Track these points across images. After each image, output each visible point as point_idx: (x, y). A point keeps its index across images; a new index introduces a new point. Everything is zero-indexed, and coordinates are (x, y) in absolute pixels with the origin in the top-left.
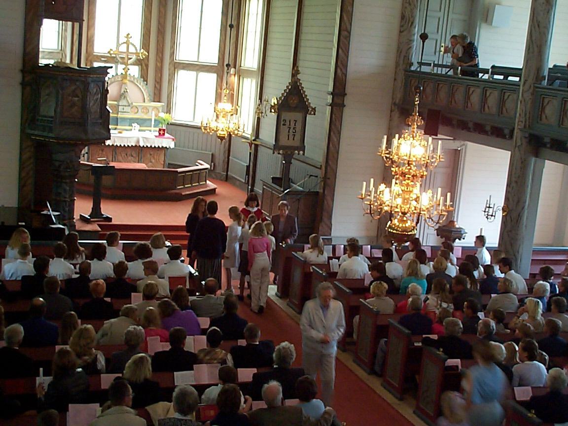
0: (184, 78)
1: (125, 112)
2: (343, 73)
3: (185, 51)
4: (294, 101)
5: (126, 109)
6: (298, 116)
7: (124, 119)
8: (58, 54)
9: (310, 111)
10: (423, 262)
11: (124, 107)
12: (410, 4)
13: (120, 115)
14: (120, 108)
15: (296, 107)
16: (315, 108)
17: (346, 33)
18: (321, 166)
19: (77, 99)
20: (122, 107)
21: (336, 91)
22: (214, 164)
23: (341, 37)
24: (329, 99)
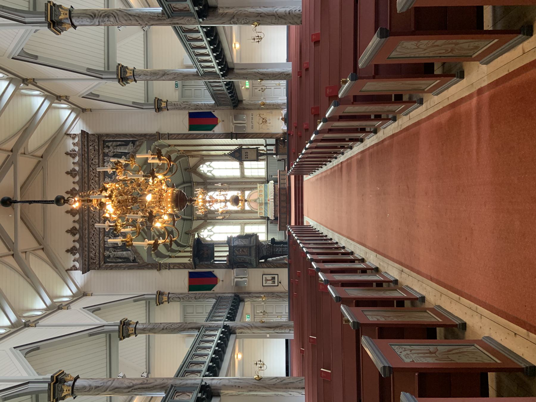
2: (222, 135)
3: (237, 173)
4: (237, 154)
5: (261, 199)
7: (265, 200)
12: (189, 107)
13: (263, 202)
14: (260, 202)
17: (205, 136)
21: (230, 137)
23: (207, 138)
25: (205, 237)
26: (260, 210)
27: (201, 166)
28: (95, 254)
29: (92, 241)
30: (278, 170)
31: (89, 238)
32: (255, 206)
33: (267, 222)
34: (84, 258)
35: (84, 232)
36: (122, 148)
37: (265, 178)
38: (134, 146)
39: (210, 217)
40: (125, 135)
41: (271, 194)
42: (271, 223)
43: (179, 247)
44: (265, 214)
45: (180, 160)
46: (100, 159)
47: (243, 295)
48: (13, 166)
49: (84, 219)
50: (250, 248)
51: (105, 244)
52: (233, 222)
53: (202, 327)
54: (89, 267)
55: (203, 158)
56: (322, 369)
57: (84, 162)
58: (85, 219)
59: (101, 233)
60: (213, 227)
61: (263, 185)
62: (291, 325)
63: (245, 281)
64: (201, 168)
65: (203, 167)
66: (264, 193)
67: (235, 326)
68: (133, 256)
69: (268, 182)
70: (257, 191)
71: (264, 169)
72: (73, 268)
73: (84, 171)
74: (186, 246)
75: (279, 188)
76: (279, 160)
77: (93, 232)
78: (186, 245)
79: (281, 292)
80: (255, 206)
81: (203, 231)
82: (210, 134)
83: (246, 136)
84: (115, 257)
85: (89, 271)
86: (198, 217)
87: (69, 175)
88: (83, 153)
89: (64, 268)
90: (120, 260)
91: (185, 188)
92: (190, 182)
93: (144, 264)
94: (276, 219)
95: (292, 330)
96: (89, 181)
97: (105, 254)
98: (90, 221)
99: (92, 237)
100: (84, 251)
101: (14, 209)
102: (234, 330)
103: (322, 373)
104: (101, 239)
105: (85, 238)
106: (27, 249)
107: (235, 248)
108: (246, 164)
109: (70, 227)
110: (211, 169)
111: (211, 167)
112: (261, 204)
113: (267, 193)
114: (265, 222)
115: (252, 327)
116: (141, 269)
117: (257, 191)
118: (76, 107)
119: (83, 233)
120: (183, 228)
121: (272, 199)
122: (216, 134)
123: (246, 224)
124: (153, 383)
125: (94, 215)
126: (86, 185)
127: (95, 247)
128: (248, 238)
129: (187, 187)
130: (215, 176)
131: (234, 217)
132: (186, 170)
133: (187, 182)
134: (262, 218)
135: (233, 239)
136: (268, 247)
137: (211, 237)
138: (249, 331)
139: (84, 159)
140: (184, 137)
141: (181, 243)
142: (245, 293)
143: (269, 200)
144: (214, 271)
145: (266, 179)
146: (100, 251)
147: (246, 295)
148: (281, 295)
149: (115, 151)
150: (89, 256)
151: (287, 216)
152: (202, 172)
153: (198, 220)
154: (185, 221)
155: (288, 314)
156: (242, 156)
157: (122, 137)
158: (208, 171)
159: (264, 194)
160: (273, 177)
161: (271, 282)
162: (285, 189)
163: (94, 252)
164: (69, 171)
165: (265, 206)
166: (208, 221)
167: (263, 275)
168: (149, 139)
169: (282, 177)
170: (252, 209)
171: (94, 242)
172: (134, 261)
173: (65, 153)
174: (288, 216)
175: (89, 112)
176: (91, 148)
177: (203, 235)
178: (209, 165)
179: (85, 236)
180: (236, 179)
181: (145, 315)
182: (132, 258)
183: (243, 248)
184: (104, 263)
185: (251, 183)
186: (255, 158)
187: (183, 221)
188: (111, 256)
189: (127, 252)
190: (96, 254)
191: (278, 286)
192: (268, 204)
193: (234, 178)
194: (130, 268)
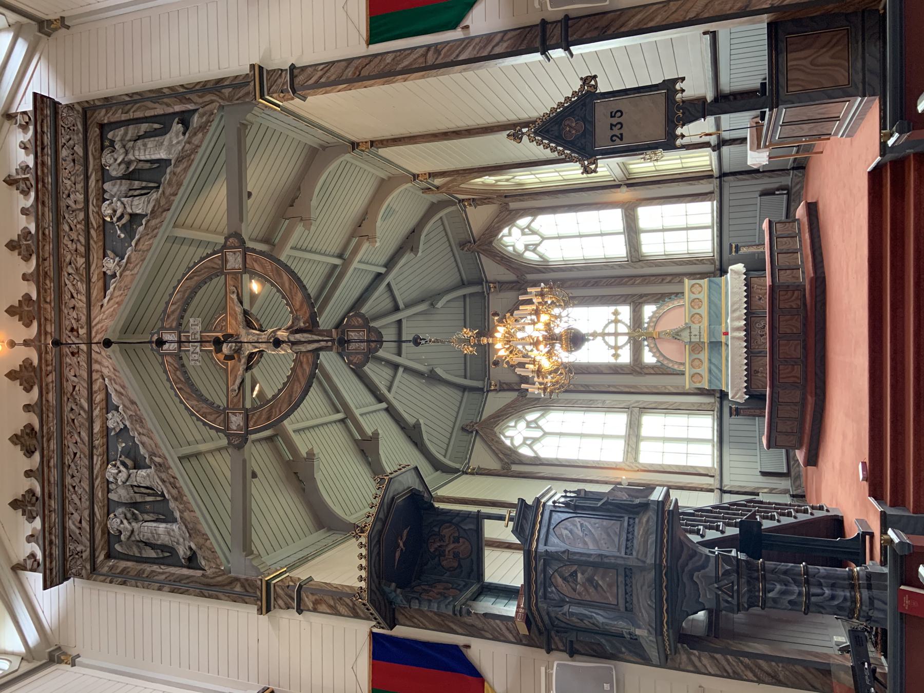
0: (651, 246)
1: (700, 333)
4: (573, 127)
6: (601, 111)
7: (711, 333)
8: (634, 413)
9: (590, 89)
10: (824, 593)
11: (692, 334)
13: (705, 339)
15: (584, 120)
16: (581, 79)
17: (430, 54)
18: (705, 33)
19: (579, 575)
20: (692, 337)
22: (778, 189)
24: (557, 54)
25: (517, 442)
26: (692, 366)
27: (505, 231)
28: (80, 522)
29: (73, 476)
30: (765, 225)
31: (63, 468)
32: (673, 352)
33: (718, 405)
34: (47, 534)
36: (150, 145)
37: (711, 261)
38: (184, 134)
40: (158, 95)
41: (733, 311)
42: (736, 411)
43: (439, 472)
44: (710, 382)
45: (442, 213)
46: (90, 190)
50: (628, 572)
51: (109, 491)
52: (604, 402)
54: (64, 565)
55: (507, 204)
57: (43, 203)
58: (47, 401)
59: (95, 451)
60: (542, 416)
61: (705, 282)
64: (505, 239)
65: (510, 234)
66: (710, 307)
69: (723, 271)
70: (681, 303)
71: (710, 231)
73: (44, 234)
74: (456, 471)
75: (772, 288)
76: (764, 193)
77: (73, 448)
78: (457, 466)
80: (672, 351)
81: (512, 424)
82: (448, 42)
83: (608, 27)
85: (66, 578)
88: (39, 173)
89: (8, 558)
90: (152, 554)
91: (468, 300)
92: (480, 282)
93: (219, 579)
94: (755, 397)
96: (59, 269)
98: (67, 409)
99: (72, 465)
100: (46, 512)
104: (95, 472)
108: (651, 423)
109: (18, 427)
110: (535, 239)
111: (534, 233)
113: (719, 308)
114: (713, 404)
116: (210, 597)
117: (681, 303)
118: (29, 21)
121: (738, 329)
122: (473, 38)
123: (644, 409)
125: (74, 387)
127: (80, 499)
129: (471, 295)
130: (548, 261)
131: (609, 386)
132: (462, 245)
133: (471, 283)
134: (701, 392)
136: (727, 573)
137: (536, 447)
139: (44, 194)
140: (349, 73)
141: (446, 461)
143: (726, 334)
144: (468, 647)
145: (718, 263)
146: (92, 514)
149: (131, 157)
150: (64, 528)
151: (804, 399)
152: (511, 249)
153: (500, 390)
154: (466, 393)
156: (593, 134)
157: (150, 104)
158: (527, 247)
159: (709, 313)
160: (744, 250)
162: (800, 288)
163: (76, 516)
165: (710, 353)
168: (230, 99)
169: (784, 244)
170: (665, 362)
171: (77, 480)
172: (192, 561)
173: (4, 181)
174: (810, 400)
175: (63, 31)
176: (64, 153)
177: (512, 438)
178: (528, 227)
180: (612, 267)
182: (182, 551)
183: (590, 570)
184: (108, 556)
185: (662, 278)
186: (658, 132)
187: (460, 394)
189: (169, 526)
190: (83, 521)
193: (608, 264)
194: (177, 587)
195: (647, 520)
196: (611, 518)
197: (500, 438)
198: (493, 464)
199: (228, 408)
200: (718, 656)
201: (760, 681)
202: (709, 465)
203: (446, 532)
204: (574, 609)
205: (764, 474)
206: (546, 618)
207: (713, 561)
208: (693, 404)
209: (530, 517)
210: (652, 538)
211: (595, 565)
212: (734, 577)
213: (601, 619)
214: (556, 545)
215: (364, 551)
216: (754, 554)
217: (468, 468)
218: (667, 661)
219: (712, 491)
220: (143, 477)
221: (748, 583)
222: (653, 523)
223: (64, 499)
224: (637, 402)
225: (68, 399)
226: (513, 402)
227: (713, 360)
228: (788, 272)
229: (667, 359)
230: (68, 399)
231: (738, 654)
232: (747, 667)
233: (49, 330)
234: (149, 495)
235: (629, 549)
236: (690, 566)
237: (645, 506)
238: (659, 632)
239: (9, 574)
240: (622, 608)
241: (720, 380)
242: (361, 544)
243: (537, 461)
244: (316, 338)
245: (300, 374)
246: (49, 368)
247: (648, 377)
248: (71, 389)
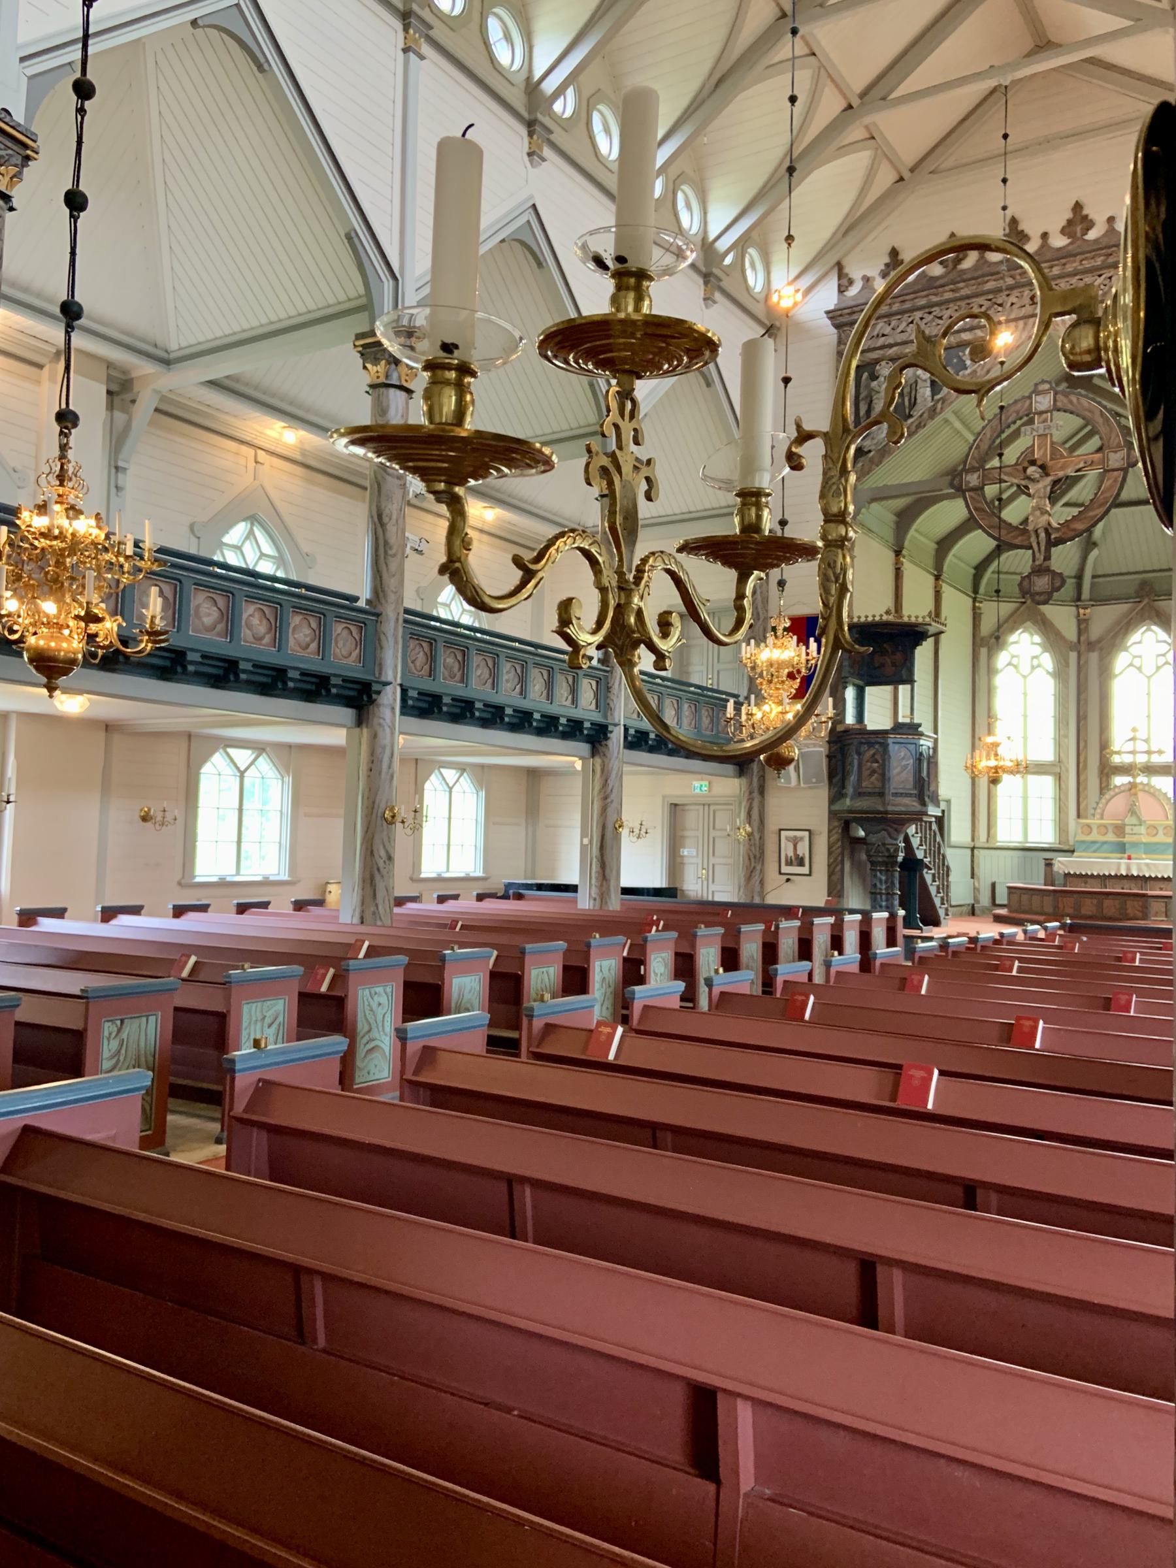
5: (1136, 829)
7: (1135, 845)
11: (1133, 827)
13: (1127, 839)
14: (1128, 829)
26: (1099, 826)
28: (883, 335)
29: (922, 319)
31: (928, 307)
35: (947, 288)
39: (1086, 662)
47: (755, 773)
48: (1128, 23)
49: (986, 279)
50: (881, 794)
52: (1066, 736)
53: (608, 669)
56: (812, 998)
58: (987, 281)
62: (606, 903)
63: (788, 780)
67: (608, 755)
68: (872, 448)
72: (845, 282)
77: (946, 314)
78: (982, 590)
79: (762, 882)
84: (873, 393)
85: (837, 326)
86: (1086, 621)
87: (887, 260)
89: (845, 255)
95: (594, 906)
97: (883, 363)
101: (1061, 46)
102: (599, 753)
103: (803, 998)
105: (927, 296)
106: (885, 139)
107: (881, 749)
108: (1045, 785)
112: (1120, 830)
115: (606, 798)
119: (942, 286)
120: (1121, 574)
123: (1059, 778)
124: (388, 570)
125: (1000, 305)
126: (1099, 261)
127: (902, 332)
128: (915, 788)
131: (1086, 742)
135: (912, 741)
136: (888, 850)
138: (597, 787)
142: (762, 778)
146: (890, 346)
147: (755, 780)
148: (756, 879)
153: (1078, 620)
155: (710, 899)
161: (791, 853)
163: (887, 330)
164: (1085, 212)
166: (1073, 656)
167: (809, 831)
179: (936, 295)
181: (714, 506)
183: (880, 771)
187: (1073, 574)
188: (874, 384)
190: (884, 338)
191: (780, 873)
192: (1119, 855)
195: (915, 806)
196: (915, 782)
197: (1017, 629)
198: (987, 626)
199: (984, 470)
200: (840, 844)
201: (829, 866)
202: (999, 839)
203: (899, 656)
204: (856, 762)
205: (993, 885)
206: (850, 742)
207: (894, 842)
208: (1067, 824)
209: (910, 731)
210: (903, 809)
211: (883, 775)
212: (887, 854)
213: (852, 778)
214: (893, 749)
215: (877, 618)
216: (902, 865)
217: (981, 602)
218: (832, 814)
219: (973, 840)
220: (924, 394)
221: (883, 862)
222: (913, 809)
223: (902, 312)
224: (1067, 771)
225: (990, 300)
226: (1063, 638)
227: (1105, 846)
228: (1164, 910)
229: (1107, 803)
230: (990, 300)
231: (842, 854)
232: (836, 859)
233: (1054, 269)
234: (910, 400)
235: (895, 795)
236: (890, 829)
237: (924, 804)
238: (850, 812)
239: (834, 261)
240: (860, 790)
241: (1084, 851)
242: (881, 616)
243: (991, 671)
244: (1043, 548)
245: (1012, 534)
246: (1018, 277)
247: (1098, 781)
248: (1000, 301)
